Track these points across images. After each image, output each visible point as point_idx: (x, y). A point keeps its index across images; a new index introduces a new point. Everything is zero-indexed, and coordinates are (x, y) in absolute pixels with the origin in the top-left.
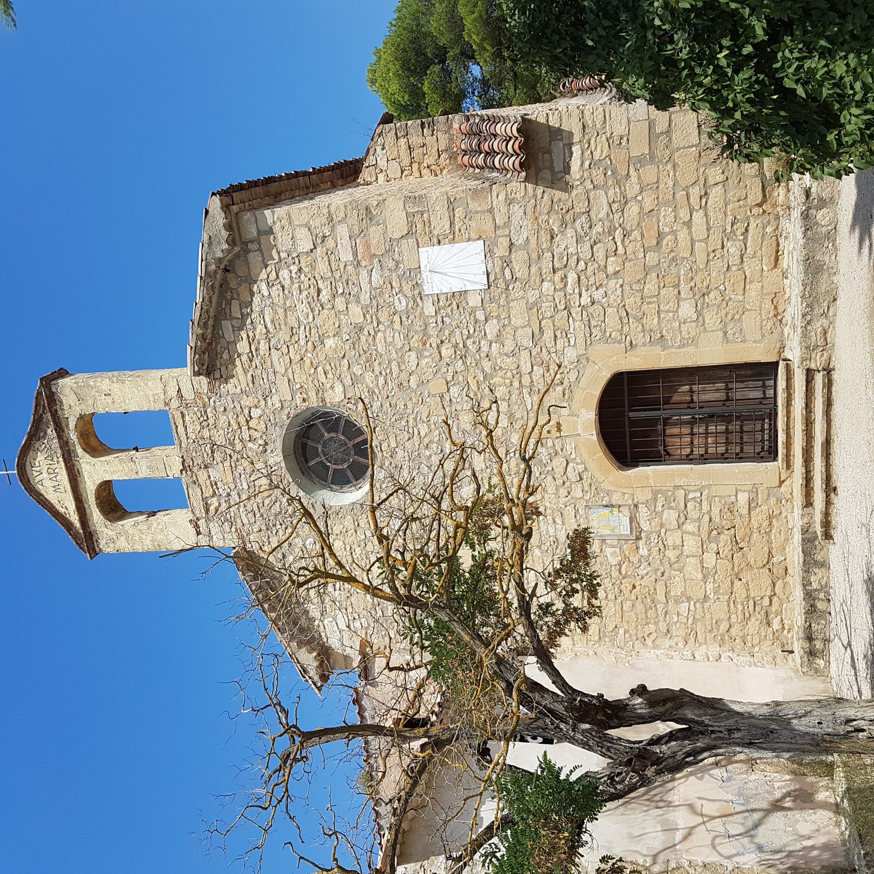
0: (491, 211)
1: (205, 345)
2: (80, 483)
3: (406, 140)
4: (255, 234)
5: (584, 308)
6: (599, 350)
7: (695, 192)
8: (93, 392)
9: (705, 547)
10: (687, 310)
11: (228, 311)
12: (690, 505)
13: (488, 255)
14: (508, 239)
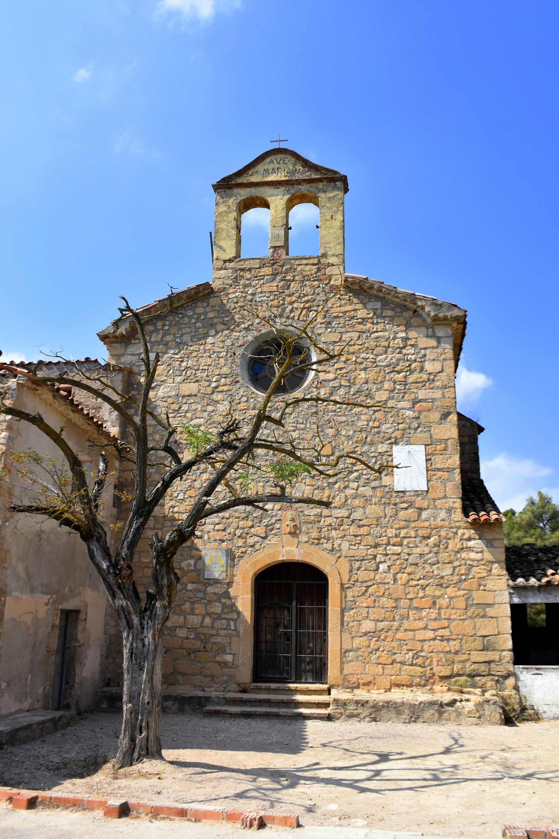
0: (445, 497)
1: (365, 288)
2: (269, 187)
3: (467, 441)
4: (438, 335)
5: (375, 557)
6: (344, 565)
7: (446, 632)
8: (335, 209)
9: (192, 630)
10: (368, 626)
11: (387, 307)
12: (224, 622)
13: (417, 493)
14: (426, 507)
